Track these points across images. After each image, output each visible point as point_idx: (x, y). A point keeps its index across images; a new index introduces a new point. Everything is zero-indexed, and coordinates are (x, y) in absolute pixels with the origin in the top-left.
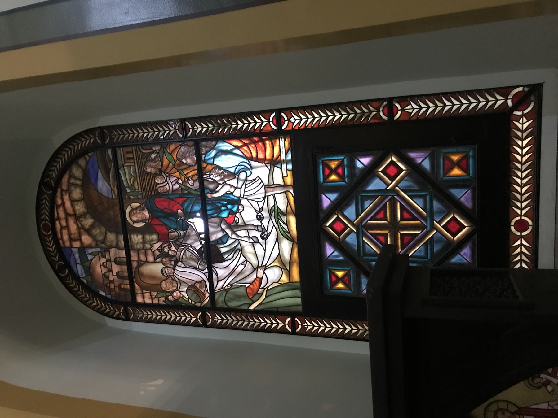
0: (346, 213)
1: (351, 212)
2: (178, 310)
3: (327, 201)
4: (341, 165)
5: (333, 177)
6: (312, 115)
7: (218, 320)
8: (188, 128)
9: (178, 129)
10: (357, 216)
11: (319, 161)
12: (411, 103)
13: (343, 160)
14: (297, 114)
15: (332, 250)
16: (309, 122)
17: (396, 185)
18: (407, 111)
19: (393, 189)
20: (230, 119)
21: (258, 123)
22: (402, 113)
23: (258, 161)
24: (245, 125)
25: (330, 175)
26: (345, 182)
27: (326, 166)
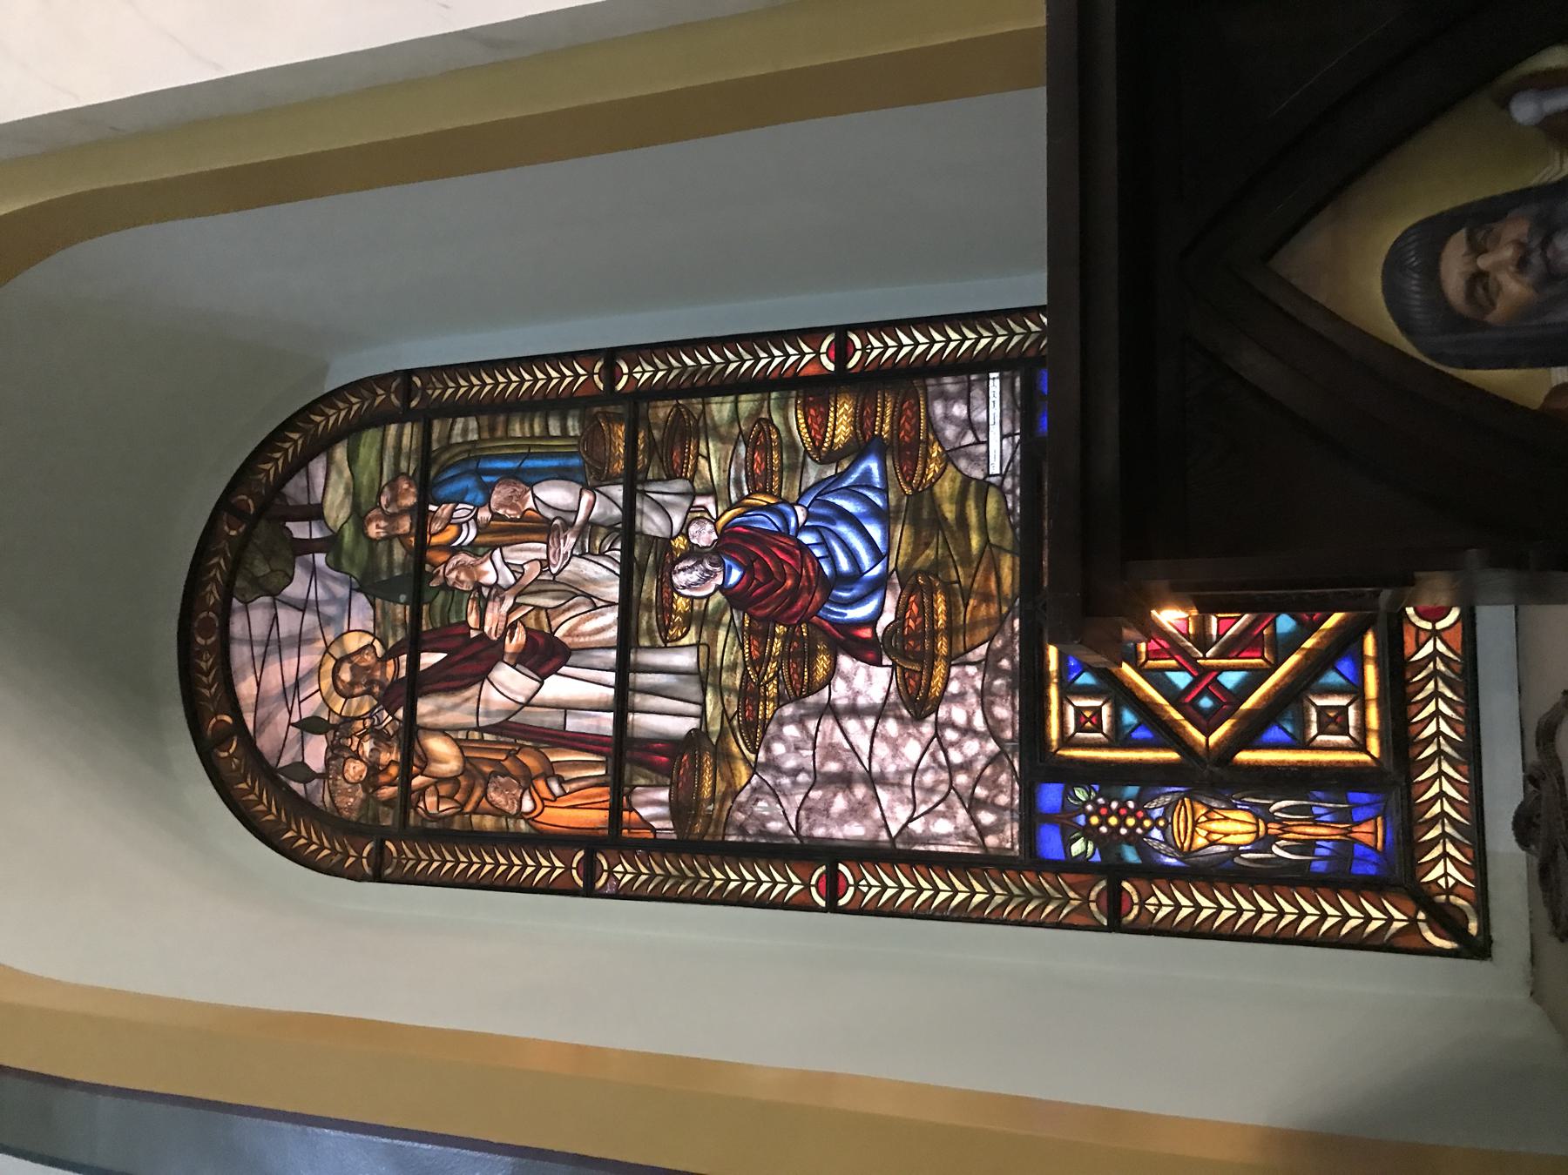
6: (481, 857)
7: (622, 878)
8: (845, 883)
9: (604, 871)
12: (623, 861)
14: (751, 869)
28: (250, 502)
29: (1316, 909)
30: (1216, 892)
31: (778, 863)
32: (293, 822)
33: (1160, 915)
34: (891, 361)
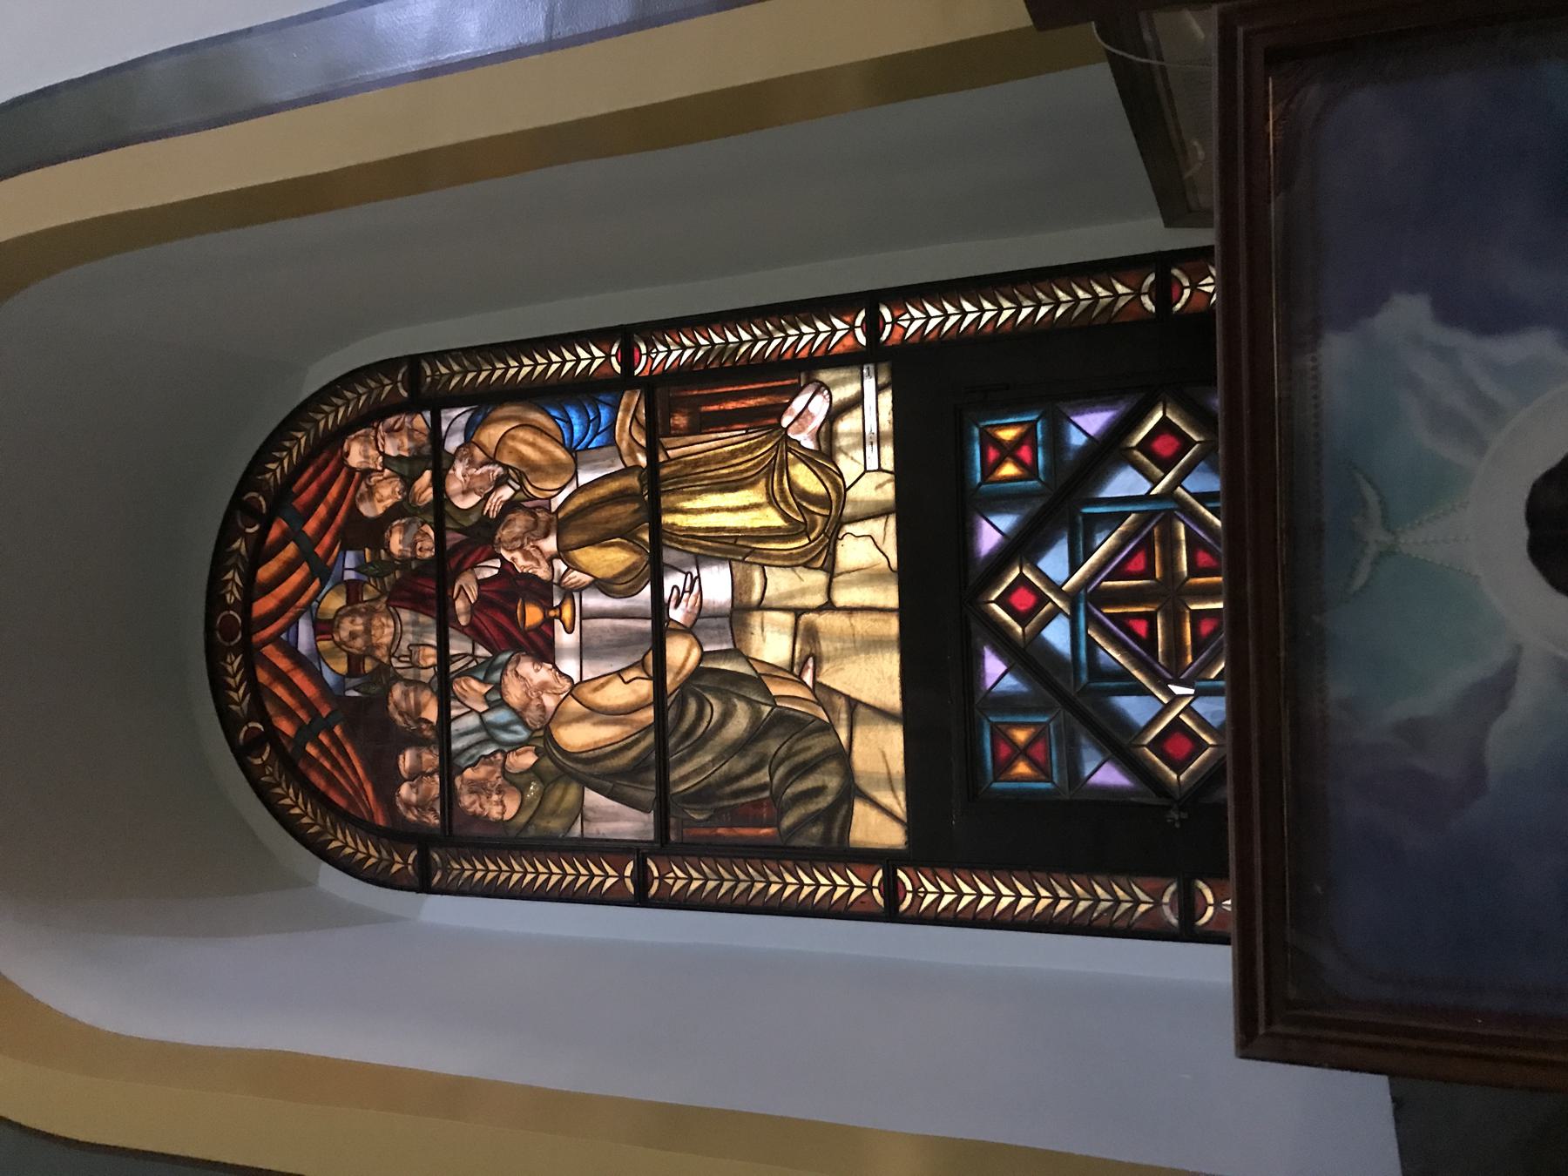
0: (1042, 565)
1: (1055, 562)
2: (916, 870)
3: (989, 536)
4: (1027, 437)
5: (1009, 470)
7: (674, 883)
10: (1074, 568)
11: (973, 430)
12: (675, 868)
13: (1034, 423)
15: (1002, 668)
16: (916, 328)
17: (1177, 481)
18: (1203, 291)
19: (1169, 493)
20: (783, 322)
21: (590, 358)
22: (1194, 297)
23: (703, 431)
24: (1004, 312)
25: (999, 463)
26: (1039, 480)
27: (989, 440)
28: (261, 498)
29: (1011, 890)
30: (815, 870)
31: (840, 867)
32: (339, 831)
33: (676, 889)
34: (954, 330)
